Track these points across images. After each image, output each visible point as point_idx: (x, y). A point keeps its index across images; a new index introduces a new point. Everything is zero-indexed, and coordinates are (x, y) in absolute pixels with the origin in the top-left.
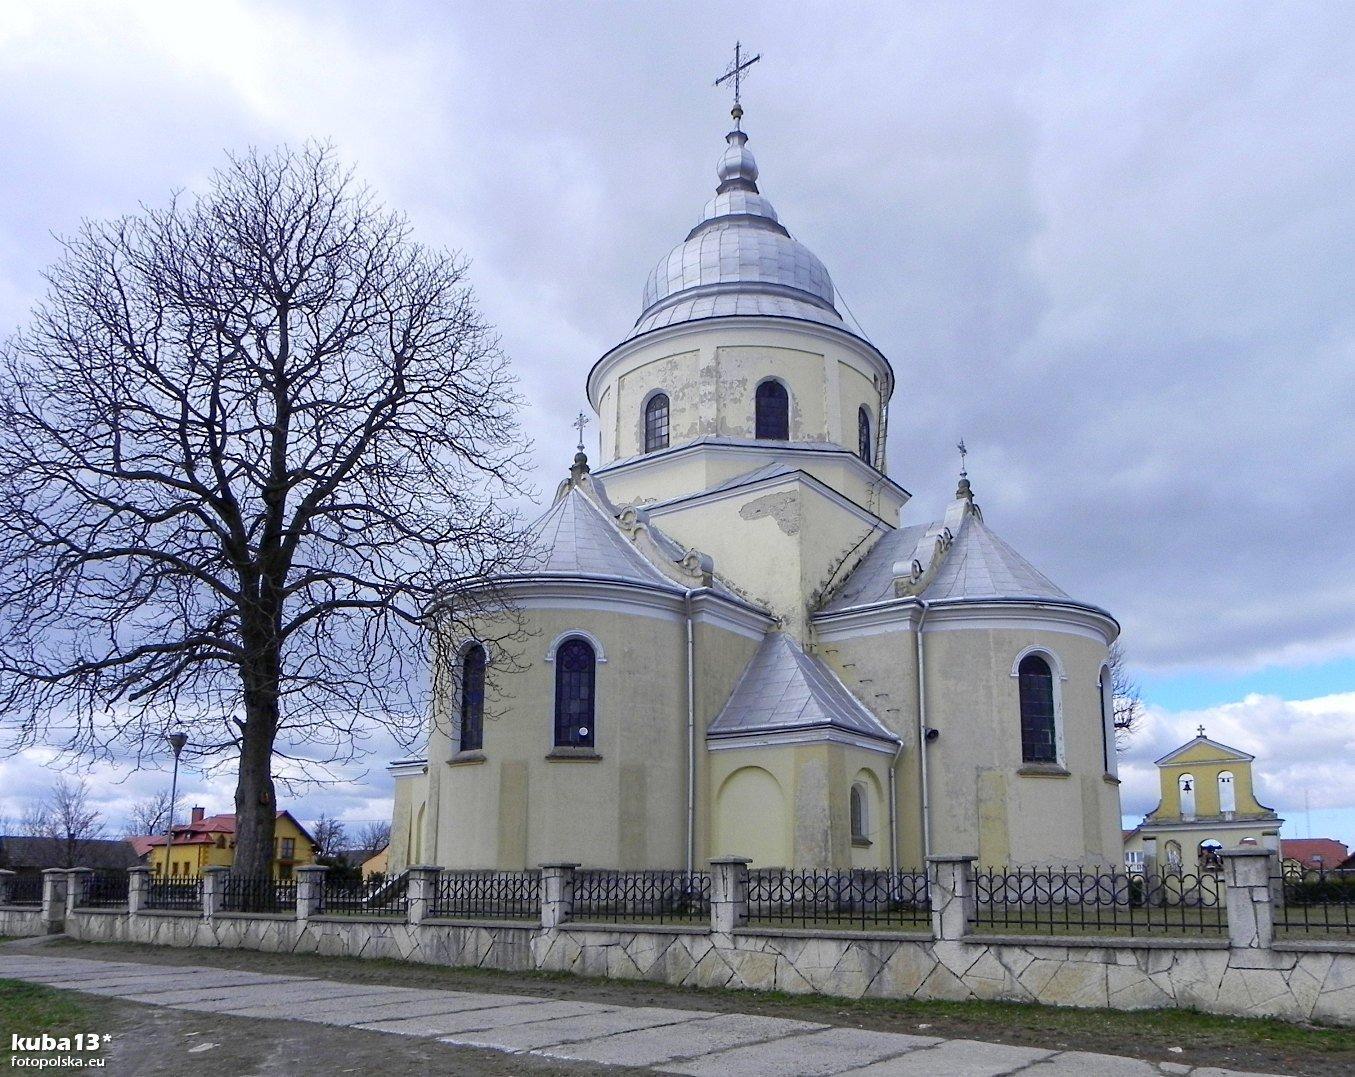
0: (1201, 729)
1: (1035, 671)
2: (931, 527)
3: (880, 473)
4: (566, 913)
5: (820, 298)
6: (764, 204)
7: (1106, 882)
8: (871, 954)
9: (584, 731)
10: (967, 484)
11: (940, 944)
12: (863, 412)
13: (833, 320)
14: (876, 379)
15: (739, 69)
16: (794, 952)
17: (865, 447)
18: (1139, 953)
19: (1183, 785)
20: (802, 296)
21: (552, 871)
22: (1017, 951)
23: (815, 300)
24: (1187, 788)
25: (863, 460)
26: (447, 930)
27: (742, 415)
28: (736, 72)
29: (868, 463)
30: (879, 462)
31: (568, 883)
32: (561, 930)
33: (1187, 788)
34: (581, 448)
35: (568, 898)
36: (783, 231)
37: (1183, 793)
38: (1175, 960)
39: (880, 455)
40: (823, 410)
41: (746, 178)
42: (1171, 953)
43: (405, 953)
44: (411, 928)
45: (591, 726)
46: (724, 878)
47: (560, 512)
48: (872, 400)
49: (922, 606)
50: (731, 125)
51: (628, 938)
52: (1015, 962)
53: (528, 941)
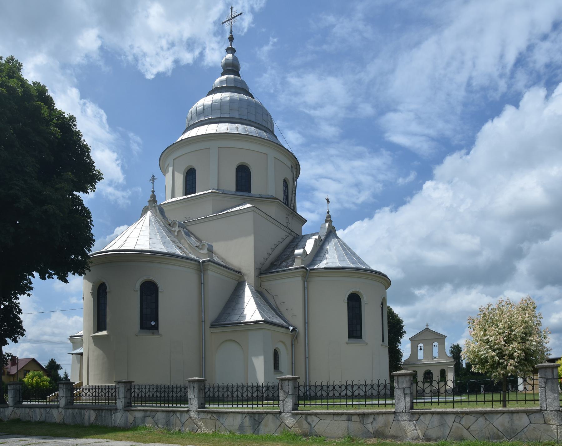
0: (427, 325)
1: (354, 301)
2: (314, 235)
3: (293, 210)
4: (128, 403)
5: (267, 128)
6: (243, 82)
7: (337, 388)
8: (255, 419)
9: (153, 323)
10: (329, 216)
11: (283, 414)
12: (285, 182)
13: (272, 138)
14: (292, 167)
15: (232, 18)
16: (223, 419)
17: (286, 198)
18: (360, 416)
19: (419, 348)
20: (258, 126)
21: (121, 384)
22: (313, 416)
23: (264, 129)
24: (421, 349)
25: (285, 204)
26: (76, 410)
27: (230, 183)
28: (231, 19)
29: (288, 205)
30: (292, 205)
31: (128, 390)
32: (125, 410)
33: (421, 349)
34: (153, 191)
35: (129, 396)
36: (251, 95)
37: (419, 351)
38: (374, 419)
39: (293, 202)
40: (264, 182)
41: (234, 69)
42: (373, 416)
43: (58, 421)
44: (60, 410)
45: (157, 320)
46: (194, 388)
47: (143, 221)
48: (289, 176)
49: (307, 270)
50: (228, 45)
51: (153, 413)
52: (313, 421)
53: (111, 415)
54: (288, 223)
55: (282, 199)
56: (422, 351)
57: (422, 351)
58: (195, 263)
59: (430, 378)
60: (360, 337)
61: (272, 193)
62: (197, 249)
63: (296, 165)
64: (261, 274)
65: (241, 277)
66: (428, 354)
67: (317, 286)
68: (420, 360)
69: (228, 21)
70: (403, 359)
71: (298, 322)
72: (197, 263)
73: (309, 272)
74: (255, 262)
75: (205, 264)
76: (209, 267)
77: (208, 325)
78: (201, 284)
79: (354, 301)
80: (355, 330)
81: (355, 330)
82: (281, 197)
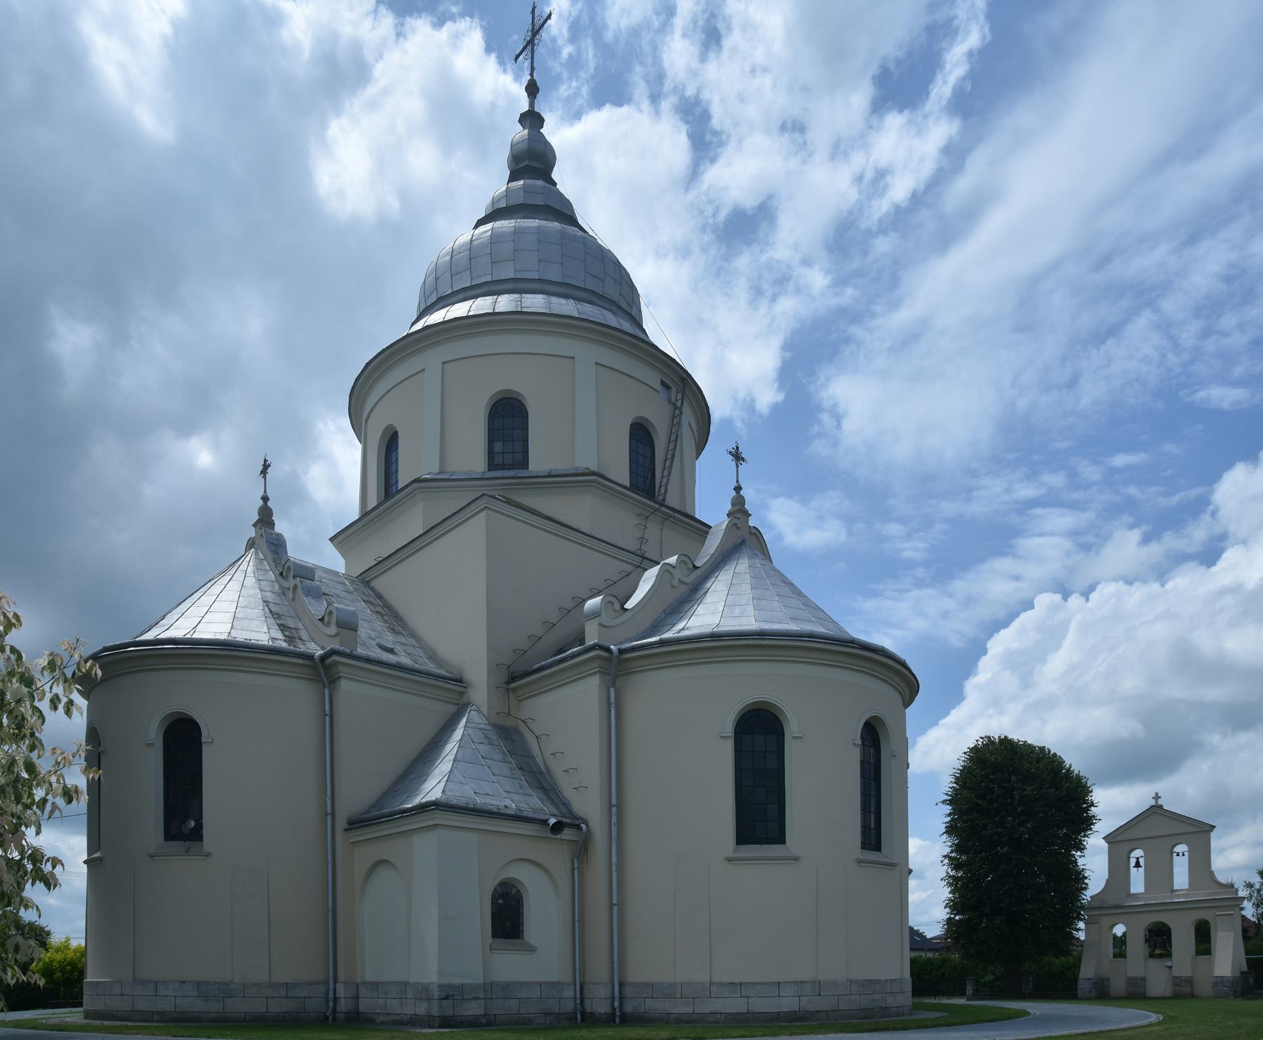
1: (759, 733)
13: (626, 326)
27: (471, 453)
33: (1138, 865)
37: (1133, 871)
49: (608, 650)
54: (642, 540)
55: (625, 479)
56: (1141, 870)
57: (1141, 870)
58: (300, 661)
59: (1164, 947)
60: (780, 839)
61: (586, 460)
62: (319, 624)
63: (683, 380)
64: (513, 678)
65: (462, 693)
66: (1160, 873)
67: (651, 693)
68: (1136, 896)
69: (525, 48)
70: (1088, 894)
71: (589, 804)
72: (308, 663)
73: (621, 662)
74: (492, 647)
75: (329, 661)
76: (340, 668)
77: (341, 823)
78: (328, 717)
79: (759, 733)
80: (760, 814)
81: (760, 814)
82: (620, 471)
